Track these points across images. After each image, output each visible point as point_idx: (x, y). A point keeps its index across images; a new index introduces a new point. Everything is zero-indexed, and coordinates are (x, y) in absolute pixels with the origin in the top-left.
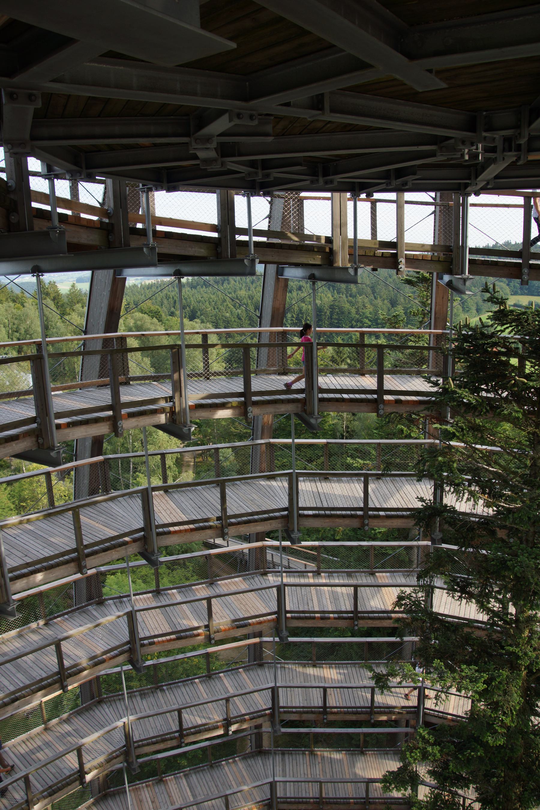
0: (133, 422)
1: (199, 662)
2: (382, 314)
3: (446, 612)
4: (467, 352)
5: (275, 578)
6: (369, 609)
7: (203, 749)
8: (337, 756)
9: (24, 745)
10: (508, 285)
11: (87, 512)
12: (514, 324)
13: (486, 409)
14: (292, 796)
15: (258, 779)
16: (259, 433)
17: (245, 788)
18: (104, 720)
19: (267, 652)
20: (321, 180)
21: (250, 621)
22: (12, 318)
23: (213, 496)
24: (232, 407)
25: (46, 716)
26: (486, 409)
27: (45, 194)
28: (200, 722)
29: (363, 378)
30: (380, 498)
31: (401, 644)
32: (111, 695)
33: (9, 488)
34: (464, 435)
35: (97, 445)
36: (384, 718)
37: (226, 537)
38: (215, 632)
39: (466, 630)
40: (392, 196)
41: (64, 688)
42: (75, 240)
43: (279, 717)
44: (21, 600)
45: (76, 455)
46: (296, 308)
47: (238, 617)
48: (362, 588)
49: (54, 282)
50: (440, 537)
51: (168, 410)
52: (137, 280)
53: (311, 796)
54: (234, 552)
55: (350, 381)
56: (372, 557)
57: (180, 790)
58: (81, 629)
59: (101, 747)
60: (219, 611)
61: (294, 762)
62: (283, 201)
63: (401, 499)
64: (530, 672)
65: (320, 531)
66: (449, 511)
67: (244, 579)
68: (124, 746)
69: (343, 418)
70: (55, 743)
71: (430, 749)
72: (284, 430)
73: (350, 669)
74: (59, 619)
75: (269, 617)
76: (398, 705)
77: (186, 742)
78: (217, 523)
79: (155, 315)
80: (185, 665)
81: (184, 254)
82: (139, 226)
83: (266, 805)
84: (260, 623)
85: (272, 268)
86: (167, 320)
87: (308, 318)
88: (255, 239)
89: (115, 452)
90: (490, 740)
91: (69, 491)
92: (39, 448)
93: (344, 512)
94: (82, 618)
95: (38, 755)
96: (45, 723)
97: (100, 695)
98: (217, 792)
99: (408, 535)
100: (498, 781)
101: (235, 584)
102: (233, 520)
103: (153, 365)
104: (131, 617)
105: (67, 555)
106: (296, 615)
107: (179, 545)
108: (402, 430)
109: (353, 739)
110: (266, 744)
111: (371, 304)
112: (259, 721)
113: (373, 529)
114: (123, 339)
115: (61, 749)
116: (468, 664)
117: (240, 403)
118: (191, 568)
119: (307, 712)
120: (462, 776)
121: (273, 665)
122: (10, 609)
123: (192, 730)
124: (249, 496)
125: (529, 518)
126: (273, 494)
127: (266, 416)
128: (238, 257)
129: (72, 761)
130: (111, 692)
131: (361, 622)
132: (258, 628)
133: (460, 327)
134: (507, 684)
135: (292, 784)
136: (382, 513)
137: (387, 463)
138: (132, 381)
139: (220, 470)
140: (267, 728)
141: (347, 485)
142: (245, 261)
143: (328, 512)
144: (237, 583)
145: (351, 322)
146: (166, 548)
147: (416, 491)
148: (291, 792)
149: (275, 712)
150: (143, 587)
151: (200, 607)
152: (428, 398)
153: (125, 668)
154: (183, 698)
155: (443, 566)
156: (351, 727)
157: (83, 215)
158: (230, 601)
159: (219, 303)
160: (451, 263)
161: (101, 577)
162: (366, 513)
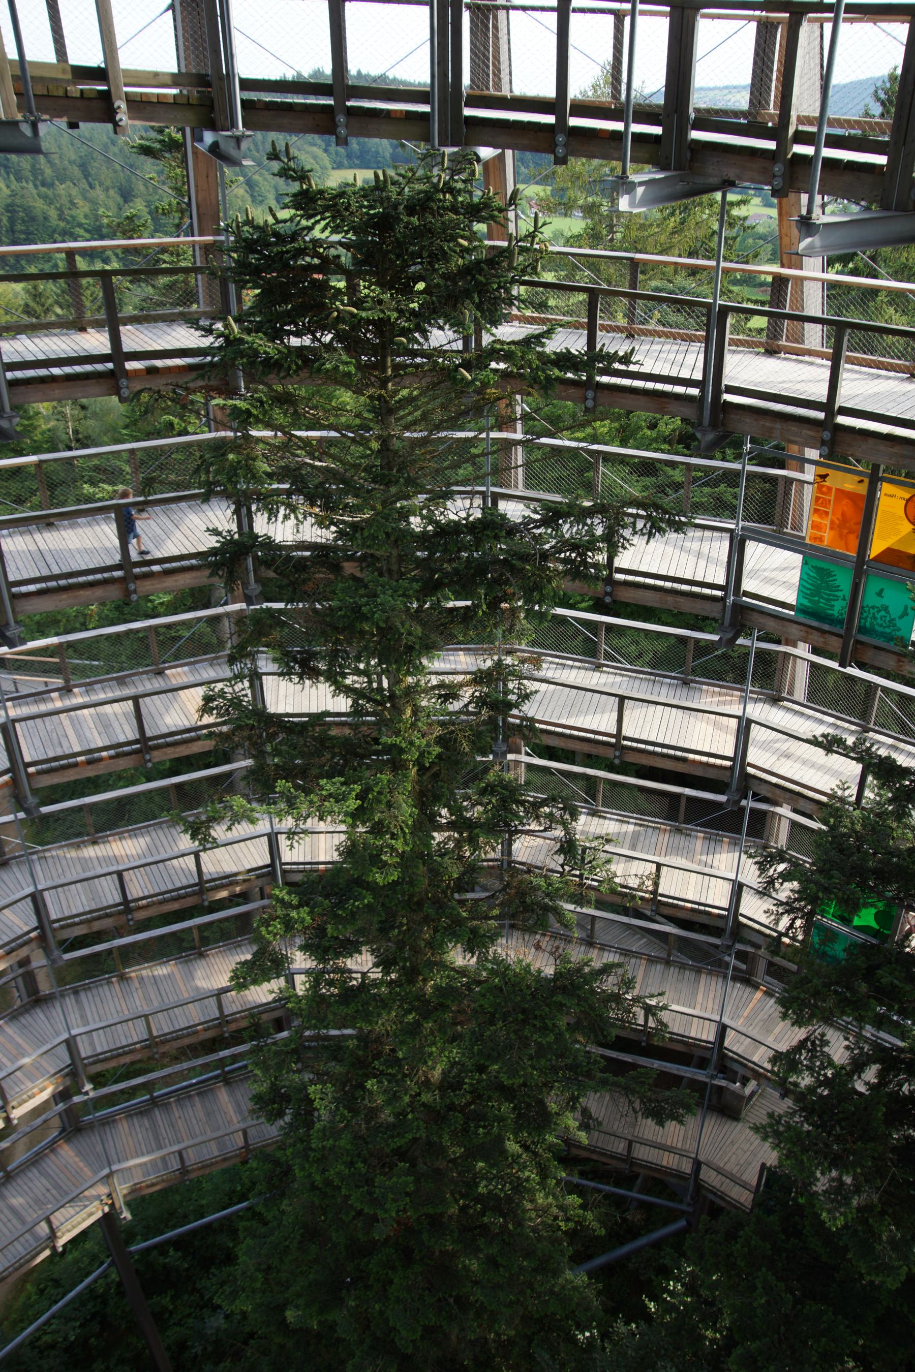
2: (108, 215)
4: (256, 272)
6: (165, 730)
10: (326, 151)
12: (327, 214)
13: (296, 364)
14: (106, 1049)
15: (43, 1042)
17: (26, 1060)
26: (296, 364)
29: (84, 335)
34: (265, 413)
36: (224, 894)
43: (54, 937)
48: (147, 699)
50: (258, 591)
53: (136, 1039)
55: (59, 342)
63: (184, 540)
64: (422, 770)
65: (59, 621)
69: (64, 416)
71: (294, 914)
73: (153, 834)
76: (241, 869)
83: (67, 1075)
90: (379, 878)
93: (91, 578)
106: (44, 766)
108: (171, 424)
109: (183, 940)
110: (45, 986)
111: (85, 198)
112: (23, 952)
113: (150, 601)
116: (330, 776)
119: (99, 918)
121: (25, 858)
125: (388, 535)
131: (155, 753)
133: (238, 226)
134: (390, 792)
135: (101, 1031)
136: (156, 568)
140: (39, 960)
141: (88, 530)
148: (102, 1044)
149: (45, 933)
160: (211, 108)
162: (128, 572)
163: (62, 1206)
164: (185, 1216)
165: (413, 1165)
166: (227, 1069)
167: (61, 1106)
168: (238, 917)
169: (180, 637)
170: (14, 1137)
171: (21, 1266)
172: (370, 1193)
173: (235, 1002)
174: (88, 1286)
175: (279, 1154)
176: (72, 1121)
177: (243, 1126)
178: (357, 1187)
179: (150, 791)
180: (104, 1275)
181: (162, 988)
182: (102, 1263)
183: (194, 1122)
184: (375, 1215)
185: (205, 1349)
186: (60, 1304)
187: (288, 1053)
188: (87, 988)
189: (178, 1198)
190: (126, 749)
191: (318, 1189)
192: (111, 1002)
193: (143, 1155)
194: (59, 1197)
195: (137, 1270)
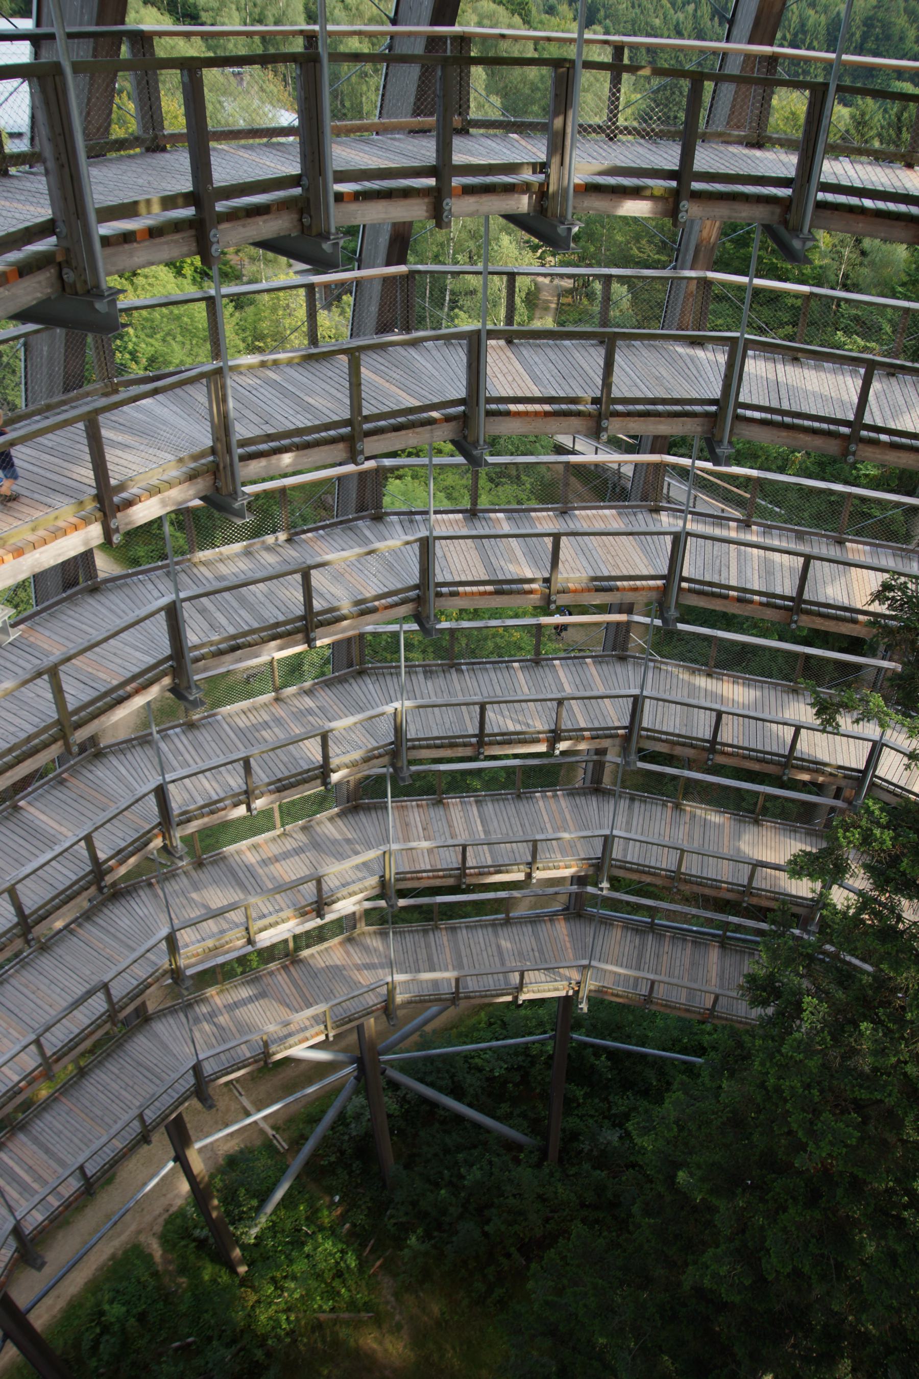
0: (469, 203)
5: (671, 520)
6: (822, 600)
7: (509, 770)
8: (715, 818)
9: (243, 717)
14: (635, 861)
15: (586, 828)
17: (566, 835)
21: (619, 583)
24: (652, 197)
25: (278, 681)
28: (511, 728)
30: (887, 409)
32: (379, 665)
33: (237, 314)
35: (400, 243)
36: (806, 777)
38: (559, 592)
41: (309, 641)
45: (360, 260)
48: (818, 563)
51: (536, 188)
53: (664, 866)
56: (845, 516)
57: (468, 821)
59: (356, 739)
61: (648, 814)
65: (759, 457)
67: (619, 514)
68: (392, 743)
69: (841, 257)
70: (289, 721)
71: (877, 832)
73: (766, 692)
74: (310, 535)
75: (652, 583)
76: (833, 762)
77: (486, 753)
78: (590, 408)
80: (498, 640)
84: (635, 589)
91: (336, 328)
92: (303, 232)
93: (816, 425)
94: (346, 538)
95: (264, 733)
96: (277, 690)
97: (362, 662)
101: (603, 518)
102: (619, 408)
104: (426, 546)
105: (334, 429)
106: (697, 586)
109: (744, 800)
110: (607, 781)
113: (856, 468)
114: (463, 40)
115: (298, 732)
118: (528, 486)
119: (684, 745)
121: (643, 660)
122: (237, 505)
126: (695, 372)
131: (804, 617)
132: (629, 597)
135: (638, 844)
136: (884, 437)
140: (613, 757)
141: (831, 377)
143: (787, 420)
144: (607, 517)
148: (633, 854)
149: (631, 735)
150: (447, 505)
151: (539, 548)
153: (406, 627)
154: (490, 688)
158: (590, 546)
161: (380, 476)
162: (855, 432)
165: (865, 1122)
166: (728, 934)
167: (574, 888)
168: (804, 803)
169: (870, 516)
171: (486, 996)
172: (812, 1123)
173: (766, 880)
174: (527, 1043)
175: (747, 1038)
176: (577, 906)
177: (718, 991)
178: (803, 1110)
179: (778, 650)
180: (542, 1043)
181: (707, 833)
182: (545, 1032)
183: (678, 963)
184: (807, 1144)
185: (592, 1150)
186: (500, 1043)
187: (801, 954)
188: (643, 801)
189: (631, 1018)
191: (766, 1089)
194: (538, 960)
195: (569, 1055)
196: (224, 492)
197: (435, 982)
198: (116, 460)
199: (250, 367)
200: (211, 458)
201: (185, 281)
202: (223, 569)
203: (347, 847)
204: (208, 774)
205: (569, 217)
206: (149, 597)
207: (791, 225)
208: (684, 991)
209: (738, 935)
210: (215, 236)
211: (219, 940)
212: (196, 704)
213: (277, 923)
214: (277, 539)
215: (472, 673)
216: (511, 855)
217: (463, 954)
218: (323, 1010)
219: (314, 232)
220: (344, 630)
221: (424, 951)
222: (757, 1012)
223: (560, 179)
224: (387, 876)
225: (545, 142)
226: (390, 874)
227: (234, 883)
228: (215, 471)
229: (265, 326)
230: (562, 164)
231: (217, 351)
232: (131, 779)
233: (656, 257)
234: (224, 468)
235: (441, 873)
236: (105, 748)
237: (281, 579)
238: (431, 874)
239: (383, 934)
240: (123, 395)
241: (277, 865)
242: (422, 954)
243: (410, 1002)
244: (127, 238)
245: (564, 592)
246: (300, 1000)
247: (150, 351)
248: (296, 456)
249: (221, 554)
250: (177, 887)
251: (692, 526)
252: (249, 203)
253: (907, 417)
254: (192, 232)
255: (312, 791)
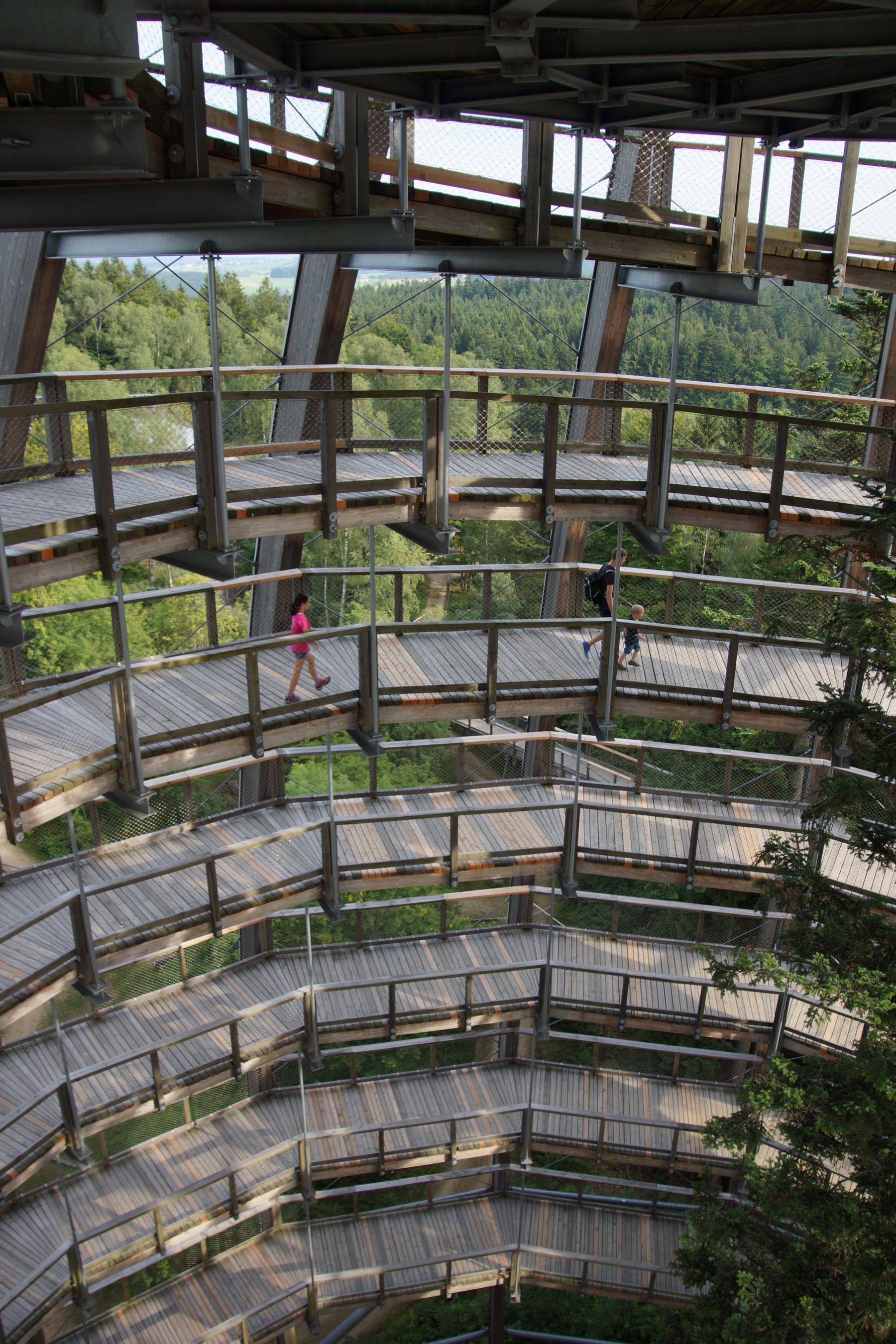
1: (429, 913)
2: (791, 363)
3: (842, 880)
5: (564, 792)
6: (714, 859)
7: (424, 1048)
8: (633, 1083)
9: (151, 1008)
11: (269, 658)
14: (556, 1134)
15: (504, 1103)
16: (562, 550)
17: (484, 1112)
18: (274, 986)
19: (540, 909)
20: (713, 110)
21: (517, 857)
22: (163, 331)
23: (477, 650)
24: (520, 503)
25: (186, 970)
27: (229, 114)
29: (748, 472)
30: (754, 678)
31: (757, 921)
32: (287, 949)
33: (145, 611)
35: (292, 550)
36: (717, 1035)
37: (493, 719)
38: (459, 869)
39: (873, 912)
40: (836, 147)
41: (215, 930)
42: (276, 199)
44: (156, 789)
45: (257, 565)
46: (640, 343)
47: (498, 850)
48: (707, 825)
49: (235, 275)
50: (847, 754)
51: (415, 500)
52: (372, 277)
53: (585, 1137)
54: (500, 744)
55: (724, 475)
56: (728, 776)
57: (383, 1103)
58: (248, 842)
59: (266, 1026)
60: (469, 837)
62: (637, 147)
63: (789, 684)
65: (645, 724)
66: (870, 713)
67: (514, 790)
68: (302, 1028)
69: (702, 538)
70: (197, 1010)
71: (788, 1091)
72: (601, 551)
73: (670, 952)
74: (214, 824)
76: (743, 1017)
77: (398, 1033)
78: (478, 693)
79: (400, 339)
80: (406, 916)
81: (459, 233)
82: (386, 179)
84: (534, 862)
85: (608, 269)
86: (420, 350)
87: (660, 362)
88: (586, 214)
89: (319, 565)
92: (199, 547)
94: (250, 826)
95: (172, 1024)
96: (184, 979)
97: (270, 947)
98: (439, 1113)
99: (792, 745)
100: (891, 1154)
101: (499, 795)
102: (505, 692)
103: (392, 426)
104: (328, 832)
105: (234, 724)
106: (593, 855)
107: (411, 724)
108: (803, 569)
109: (661, 1061)
111: (772, 346)
112: (517, 1015)
113: (735, 730)
114: (345, 376)
115: (206, 1021)
116: (871, 966)
117: (537, 496)
118: (428, 764)
119: (594, 1011)
120: (833, 1138)
121: (548, 931)
122: (139, 801)
123: (409, 1017)
124: (535, 655)
127: (573, 523)
128: (553, 244)
129: (221, 1040)
130: (286, 944)
131: (698, 878)
132: (528, 870)
135: (557, 1116)
136: (754, 704)
137: (775, 621)
138: (357, 447)
139: (489, 610)
140: (526, 1028)
142: (565, 251)
144: (502, 794)
145: (732, 375)
146: (391, 727)
147: (816, 674)
148: (554, 1127)
149: (542, 1006)
150: (349, 786)
151: (438, 827)
152: (858, 517)
153: (312, 910)
154: (398, 967)
155: (849, 803)
156: (660, 1042)
157: (290, 155)
158: (488, 822)
159: (509, 326)
161: (283, 764)
162: (727, 701)
163: (466, 1258)
164: (567, 1326)
166: (659, 1203)
169: (755, 774)
170: (447, 1174)
171: (413, 1292)
175: (685, 1324)
176: (501, 1185)
177: (654, 1267)
181: (626, 1100)
182: (478, 1328)
183: (610, 1240)
187: (730, 1225)
188: (560, 1070)
189: (567, 1304)
190: (673, 864)
192: (576, 1092)
193: (552, 1247)
196: (127, 788)
197: (358, 1281)
198: (21, 760)
199: (153, 669)
200: (114, 756)
201: (95, 582)
202: (129, 861)
203: (260, 1139)
204: (114, 1070)
205: (446, 524)
206: (54, 891)
207: (648, 522)
208: (619, 1270)
209: (669, 1204)
210: (116, 553)
211: (126, 1249)
212: (102, 999)
213: (188, 1227)
214: (182, 829)
215: (380, 954)
216: (429, 1136)
217: (387, 1247)
218: (238, 1322)
219: (209, 546)
220: (249, 918)
221: (345, 1246)
222: (694, 1290)
223: (437, 490)
224: (303, 1168)
225: (421, 457)
226: (306, 1165)
227: (142, 1184)
228: (118, 768)
229: (172, 622)
230: (437, 478)
231: (121, 654)
232: (33, 1079)
233: (535, 546)
234: (127, 765)
235: (358, 1161)
236: (7, 1046)
237: (187, 870)
238: (348, 1162)
239: (301, 1230)
240: (30, 697)
241: (188, 1162)
242: (344, 1250)
243: (332, 1306)
244: (33, 557)
245: (464, 869)
246: (214, 1312)
247: (62, 647)
248: (198, 752)
249: (126, 845)
250: (81, 1193)
251: (584, 797)
252: (149, 523)
253: (773, 683)
254: (95, 551)
255: (220, 1082)
